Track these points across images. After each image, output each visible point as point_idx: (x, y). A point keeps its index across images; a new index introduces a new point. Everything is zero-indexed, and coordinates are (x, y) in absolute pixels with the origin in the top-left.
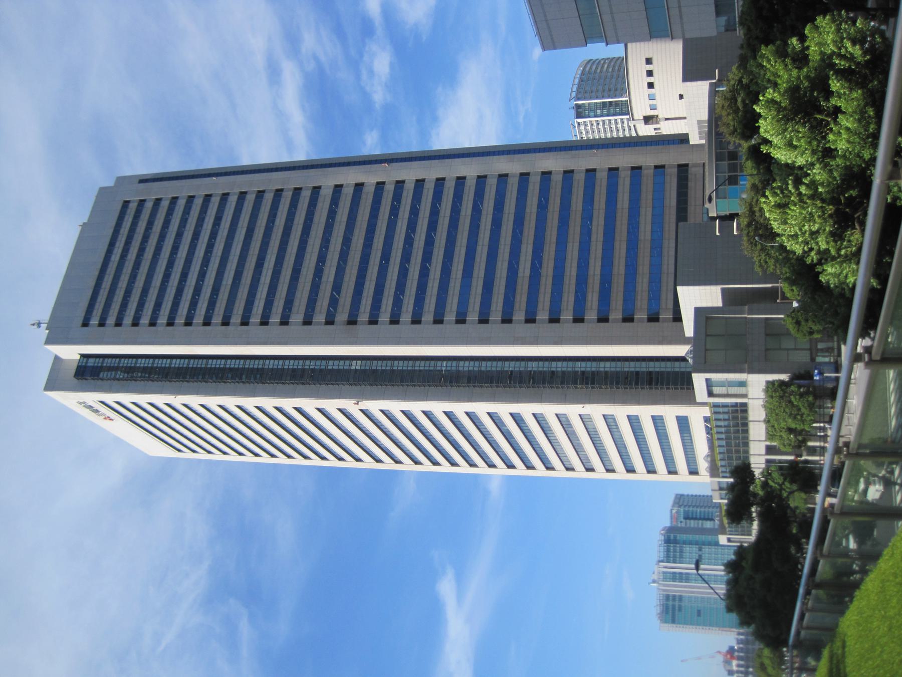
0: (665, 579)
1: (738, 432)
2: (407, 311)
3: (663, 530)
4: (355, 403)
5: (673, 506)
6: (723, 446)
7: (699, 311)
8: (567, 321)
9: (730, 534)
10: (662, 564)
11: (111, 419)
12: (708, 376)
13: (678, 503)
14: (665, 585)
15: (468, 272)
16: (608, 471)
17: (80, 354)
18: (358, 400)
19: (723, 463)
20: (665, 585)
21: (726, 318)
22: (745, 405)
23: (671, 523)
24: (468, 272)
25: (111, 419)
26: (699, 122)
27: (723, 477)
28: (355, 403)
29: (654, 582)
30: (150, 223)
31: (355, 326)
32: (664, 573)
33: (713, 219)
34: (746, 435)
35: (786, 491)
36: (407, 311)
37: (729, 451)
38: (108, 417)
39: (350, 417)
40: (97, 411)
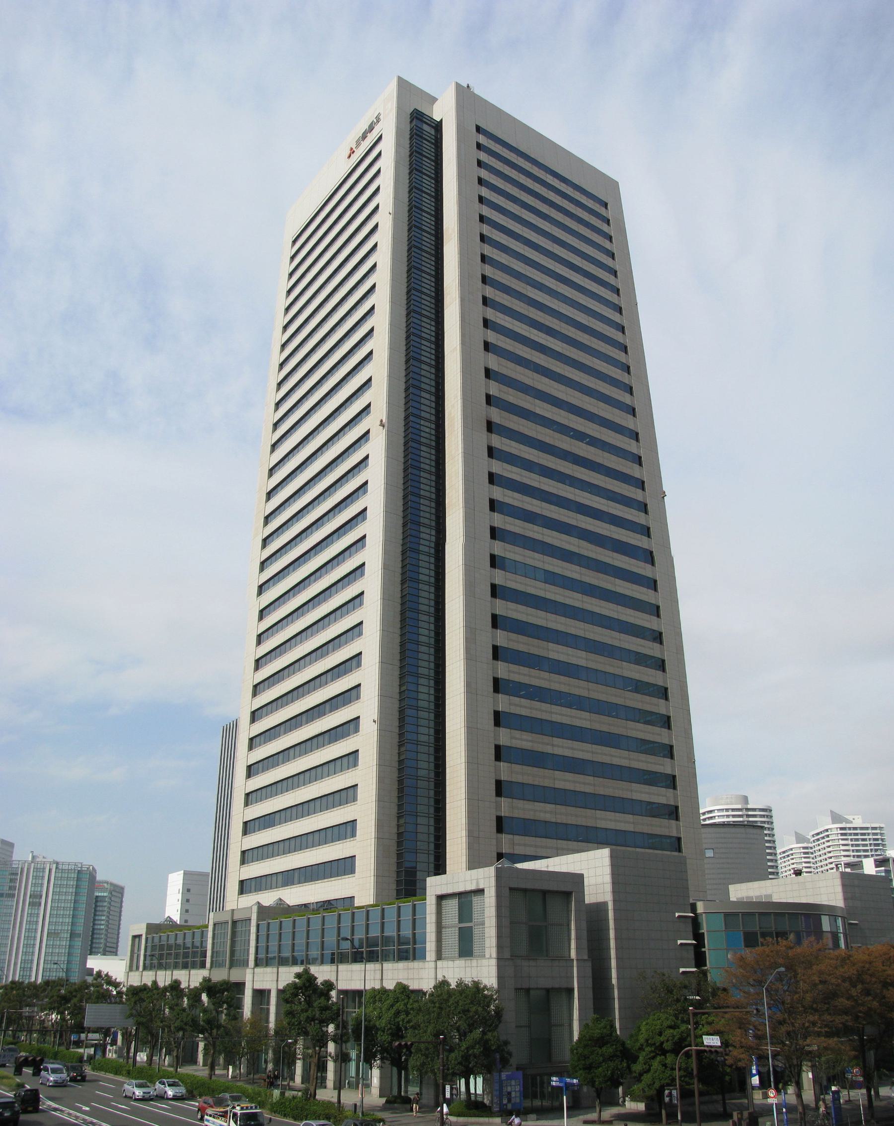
0: (36, 869)
1: (177, 956)
2: (506, 496)
3: (93, 868)
4: (382, 421)
5: (112, 884)
6: (176, 940)
7: (578, 879)
8: (495, 702)
9: (147, 939)
10: (54, 866)
11: (349, 157)
12: (144, 937)
13: (114, 891)
14: (28, 869)
15: (551, 578)
16: (249, 767)
17: (442, 120)
18: (386, 426)
19: (164, 938)
20: (28, 869)
21: (569, 925)
22: (423, 957)
23: (98, 882)
24: (551, 578)
25: (349, 157)
26: (770, 896)
27: (258, 926)
28: (382, 421)
29: (33, 857)
30: (587, 225)
31: (486, 429)
32: (44, 869)
33: (693, 908)
34: (198, 966)
35: (799, 1096)
36: (506, 496)
37: (170, 947)
38: (354, 152)
39: (354, 422)
40: (364, 137)
